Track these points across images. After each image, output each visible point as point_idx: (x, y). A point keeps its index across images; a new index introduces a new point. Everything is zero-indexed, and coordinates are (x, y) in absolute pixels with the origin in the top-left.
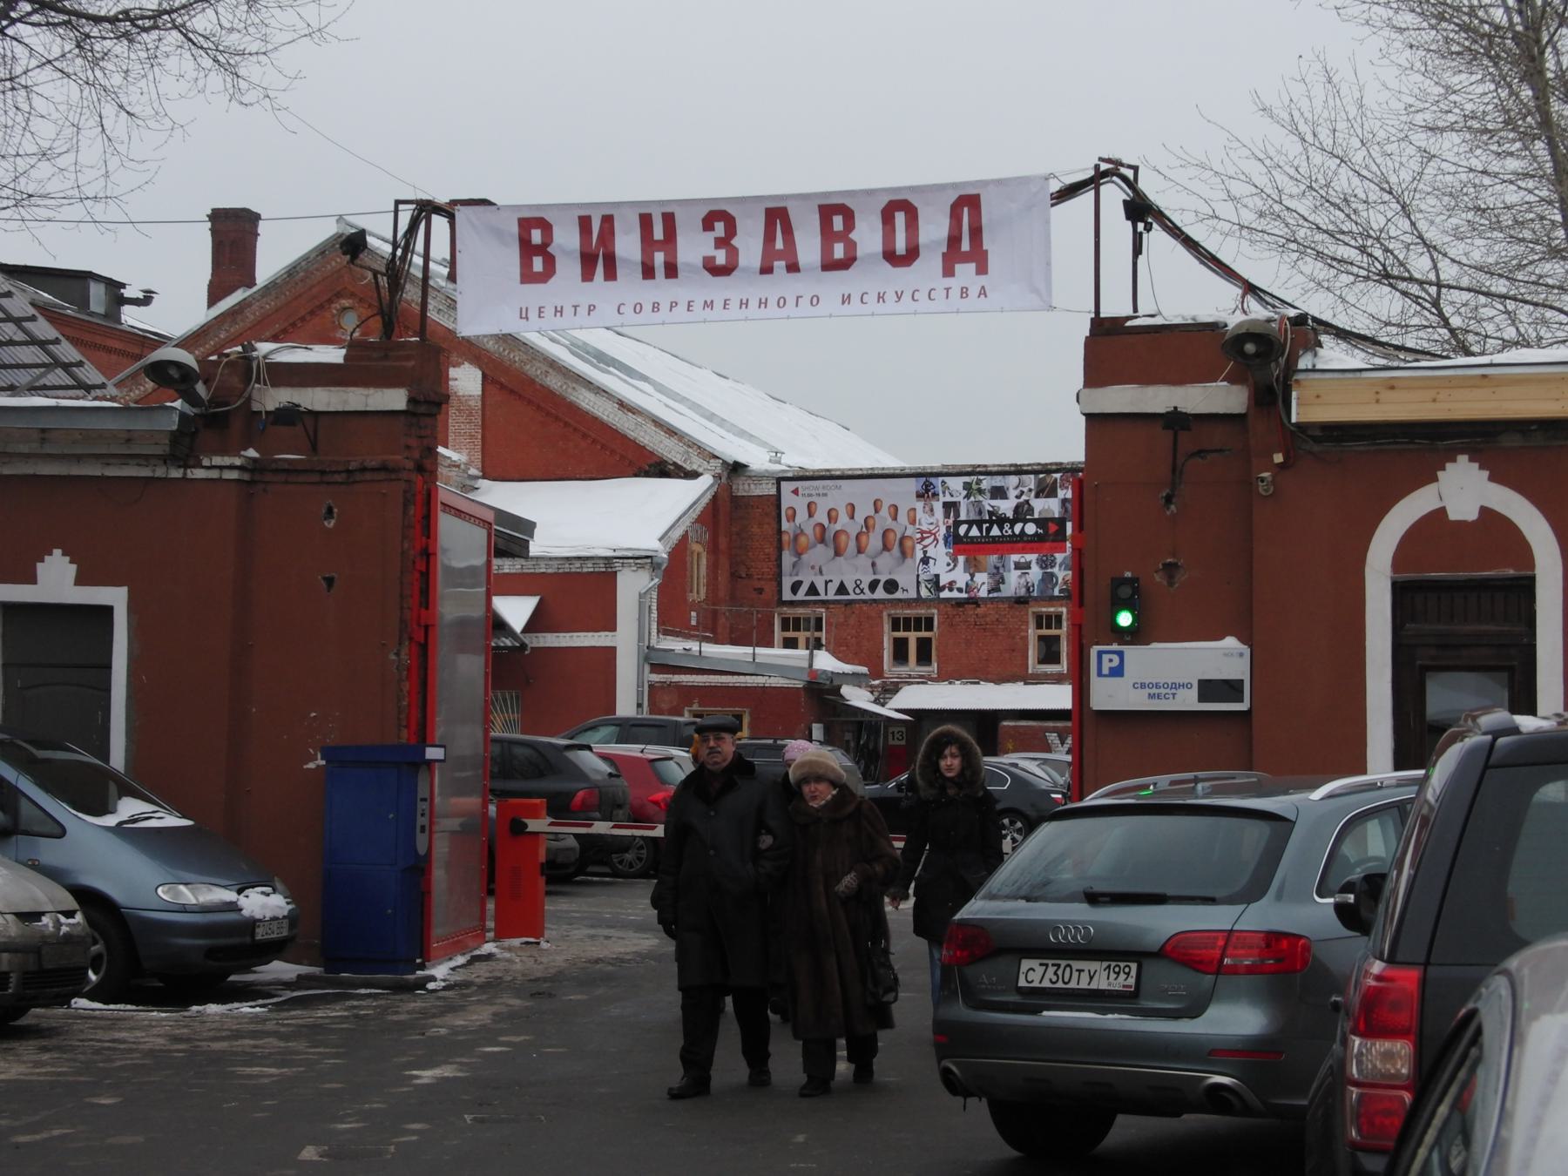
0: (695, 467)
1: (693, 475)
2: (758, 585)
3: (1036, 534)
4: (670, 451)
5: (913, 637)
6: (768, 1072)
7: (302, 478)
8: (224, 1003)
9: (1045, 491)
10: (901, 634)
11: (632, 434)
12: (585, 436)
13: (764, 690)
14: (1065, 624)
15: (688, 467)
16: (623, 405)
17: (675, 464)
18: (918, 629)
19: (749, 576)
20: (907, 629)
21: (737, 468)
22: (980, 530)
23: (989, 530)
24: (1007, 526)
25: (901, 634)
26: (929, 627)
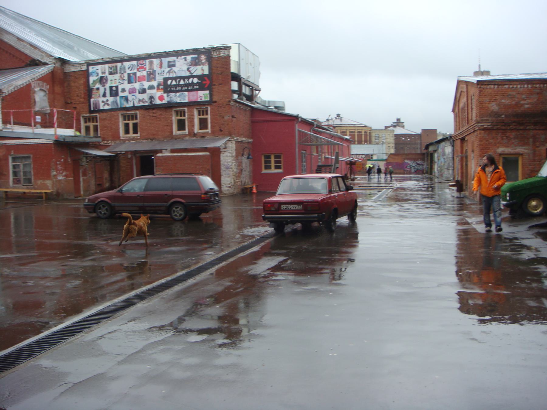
0: (45, 61)
1: (45, 64)
2: (75, 106)
3: (198, 83)
4: (37, 56)
5: (131, 123)
6: (457, 257)
7: (464, 171)
8: (239, 258)
9: (196, 63)
10: (127, 122)
11: (22, 50)
12: (7, 52)
13: (38, 145)
14: (186, 114)
15: (43, 61)
16: (19, 39)
17: (38, 60)
18: (133, 120)
19: (71, 103)
20: (129, 120)
21: (63, 62)
22: (176, 82)
23: (179, 81)
24: (186, 80)
25: (127, 122)
26: (136, 119)
